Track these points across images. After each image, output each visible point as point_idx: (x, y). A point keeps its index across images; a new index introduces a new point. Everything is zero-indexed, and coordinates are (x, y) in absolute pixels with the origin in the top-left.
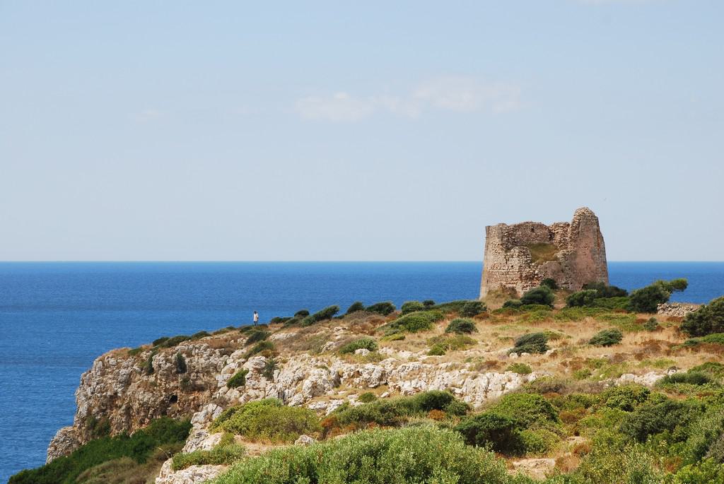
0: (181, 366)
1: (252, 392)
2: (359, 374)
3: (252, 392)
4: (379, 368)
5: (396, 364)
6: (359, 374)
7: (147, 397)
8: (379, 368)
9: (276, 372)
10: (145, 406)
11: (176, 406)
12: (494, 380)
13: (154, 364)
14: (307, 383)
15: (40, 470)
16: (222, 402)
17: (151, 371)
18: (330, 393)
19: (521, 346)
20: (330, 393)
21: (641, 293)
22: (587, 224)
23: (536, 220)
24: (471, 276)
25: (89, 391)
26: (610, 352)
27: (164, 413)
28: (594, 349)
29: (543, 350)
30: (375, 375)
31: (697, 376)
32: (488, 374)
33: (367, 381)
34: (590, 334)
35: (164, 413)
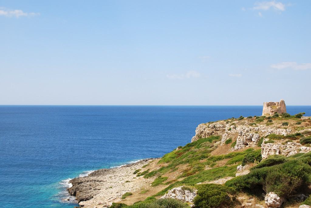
0: (214, 127)
1: (232, 131)
2: (254, 129)
3: (232, 131)
4: (258, 128)
5: (261, 127)
6: (254, 129)
7: (208, 132)
8: (258, 128)
9: (236, 128)
10: (208, 133)
11: (213, 133)
12: (280, 130)
13: (210, 126)
15: (274, 165)
16: (227, 133)
17: (209, 127)
18: (250, 132)
19: (283, 124)
20: (250, 132)
21: (298, 115)
22: (283, 102)
23: (273, 102)
24: (260, 109)
25: (198, 130)
27: (212, 135)
28: (297, 125)
29: (287, 125)
30: (257, 129)
31: (306, 131)
32: (279, 129)
33: (256, 130)
35: (212, 135)
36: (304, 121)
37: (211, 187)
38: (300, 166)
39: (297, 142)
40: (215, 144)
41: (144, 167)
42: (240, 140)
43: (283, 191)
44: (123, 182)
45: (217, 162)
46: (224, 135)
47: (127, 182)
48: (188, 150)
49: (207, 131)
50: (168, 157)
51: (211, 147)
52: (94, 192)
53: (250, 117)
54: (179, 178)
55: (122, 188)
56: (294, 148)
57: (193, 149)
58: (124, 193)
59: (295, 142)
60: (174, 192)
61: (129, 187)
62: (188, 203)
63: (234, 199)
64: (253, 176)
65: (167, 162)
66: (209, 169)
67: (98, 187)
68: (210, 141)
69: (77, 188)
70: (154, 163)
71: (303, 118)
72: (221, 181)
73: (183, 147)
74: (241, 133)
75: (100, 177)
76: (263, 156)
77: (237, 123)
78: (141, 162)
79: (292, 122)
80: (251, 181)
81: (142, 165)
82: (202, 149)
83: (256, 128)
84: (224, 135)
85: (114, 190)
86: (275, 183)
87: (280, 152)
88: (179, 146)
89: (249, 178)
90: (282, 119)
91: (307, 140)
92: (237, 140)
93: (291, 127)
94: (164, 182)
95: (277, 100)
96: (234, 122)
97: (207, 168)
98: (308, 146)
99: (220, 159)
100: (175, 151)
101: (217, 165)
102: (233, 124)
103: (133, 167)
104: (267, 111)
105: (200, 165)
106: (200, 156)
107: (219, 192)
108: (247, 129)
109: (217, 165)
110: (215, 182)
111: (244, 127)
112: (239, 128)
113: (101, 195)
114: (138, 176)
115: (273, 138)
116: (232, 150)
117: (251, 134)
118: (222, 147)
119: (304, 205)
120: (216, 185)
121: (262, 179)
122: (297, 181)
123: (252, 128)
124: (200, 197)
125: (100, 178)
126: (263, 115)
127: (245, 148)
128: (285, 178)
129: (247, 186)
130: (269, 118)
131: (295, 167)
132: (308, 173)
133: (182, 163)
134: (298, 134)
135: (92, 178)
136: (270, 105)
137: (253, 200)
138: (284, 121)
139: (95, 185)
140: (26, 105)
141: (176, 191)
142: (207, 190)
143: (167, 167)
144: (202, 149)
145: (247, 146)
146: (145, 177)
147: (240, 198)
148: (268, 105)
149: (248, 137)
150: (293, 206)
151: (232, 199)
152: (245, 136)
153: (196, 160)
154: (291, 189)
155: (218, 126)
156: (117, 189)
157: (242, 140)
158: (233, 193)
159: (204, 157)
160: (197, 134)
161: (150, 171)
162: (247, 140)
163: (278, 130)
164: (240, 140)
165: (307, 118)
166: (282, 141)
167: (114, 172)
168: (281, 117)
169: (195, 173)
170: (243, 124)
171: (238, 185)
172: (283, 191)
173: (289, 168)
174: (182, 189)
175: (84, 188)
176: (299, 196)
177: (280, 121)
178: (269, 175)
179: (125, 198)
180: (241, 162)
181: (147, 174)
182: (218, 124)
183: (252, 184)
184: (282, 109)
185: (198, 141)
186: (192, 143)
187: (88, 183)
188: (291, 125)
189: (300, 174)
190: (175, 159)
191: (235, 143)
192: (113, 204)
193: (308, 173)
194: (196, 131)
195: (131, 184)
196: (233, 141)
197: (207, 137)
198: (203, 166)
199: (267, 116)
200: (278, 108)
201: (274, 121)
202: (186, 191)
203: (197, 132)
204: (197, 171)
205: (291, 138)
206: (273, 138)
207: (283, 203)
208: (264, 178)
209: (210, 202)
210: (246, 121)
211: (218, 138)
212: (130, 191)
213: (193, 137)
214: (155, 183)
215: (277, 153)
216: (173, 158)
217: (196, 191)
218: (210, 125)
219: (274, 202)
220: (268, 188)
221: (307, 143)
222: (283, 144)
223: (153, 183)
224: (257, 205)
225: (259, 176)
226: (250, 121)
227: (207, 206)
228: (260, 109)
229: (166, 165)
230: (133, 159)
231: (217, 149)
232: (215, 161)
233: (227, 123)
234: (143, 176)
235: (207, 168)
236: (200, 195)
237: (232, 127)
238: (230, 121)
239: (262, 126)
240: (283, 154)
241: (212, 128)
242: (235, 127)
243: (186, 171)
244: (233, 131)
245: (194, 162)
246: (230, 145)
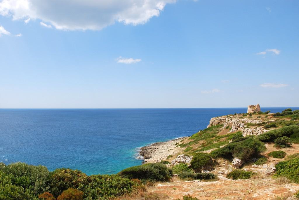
10: (217, 123)
14: (237, 121)
19: (258, 117)
22: (258, 105)
24: (246, 110)
26: (266, 118)
34: (264, 116)
36: (269, 115)
37: (201, 155)
38: (254, 142)
39: (263, 127)
40: (220, 129)
41: (181, 141)
42: (234, 127)
43: (243, 157)
44: (169, 149)
45: (220, 139)
46: (225, 124)
47: (171, 149)
48: (205, 132)
49: (216, 122)
50: (194, 136)
51: (218, 131)
52: (153, 154)
53: (240, 114)
54: (199, 148)
55: (168, 152)
56: (260, 131)
57: (208, 132)
58: (168, 155)
59: (261, 127)
60: (180, 157)
61: (172, 153)
62: (187, 164)
63: (215, 161)
64: (227, 148)
65: (193, 139)
66: (216, 143)
67: (155, 152)
68: (218, 127)
69: (145, 152)
70: (186, 139)
71: (269, 114)
72: (209, 152)
73: (203, 130)
74: (234, 123)
75: (157, 146)
76: (243, 135)
77: (233, 117)
78: (180, 139)
79: (262, 116)
80: (225, 151)
81: (180, 140)
82: (213, 132)
83: (243, 120)
84: (225, 124)
85: (164, 154)
86: (239, 152)
87: (252, 133)
88: (200, 130)
89: (224, 149)
90: (257, 115)
91: (268, 126)
92: (232, 126)
93: (262, 119)
94: (191, 150)
95: (255, 104)
96: (231, 117)
97: (215, 142)
98: (268, 130)
99: (222, 137)
100: (198, 133)
101: (221, 140)
102: (230, 118)
103: (175, 142)
104: (250, 110)
105: (211, 141)
106: (211, 136)
107: (205, 157)
108: (238, 120)
109: (221, 140)
110: (205, 152)
111: (236, 119)
112: (233, 120)
113: (156, 156)
114: (177, 146)
115: (250, 125)
116: (229, 132)
117: (240, 123)
118: (223, 131)
119: (255, 165)
120: (204, 153)
121: (231, 150)
122: (251, 151)
123: (240, 120)
124: (194, 160)
125: (157, 147)
126: (248, 112)
127: (236, 131)
128: (245, 149)
129: (223, 154)
130: (250, 114)
131: (251, 143)
132: (258, 146)
133: (201, 139)
134: (264, 123)
135: (153, 147)
136: (252, 107)
137: (226, 162)
138: (258, 116)
139: (154, 151)
140: (232, 108)
141: (181, 157)
142: (199, 156)
143: (193, 142)
144: (213, 132)
145: (238, 130)
146: (181, 147)
147: (219, 161)
148: (250, 107)
149: (238, 125)
150: (249, 166)
151: (214, 162)
152: (236, 125)
153: (209, 138)
154: (248, 155)
155: (222, 119)
156: (166, 153)
157: (235, 127)
158: (215, 158)
159: (213, 136)
160: (210, 123)
161: (184, 144)
162: (237, 126)
163: (255, 121)
164: (234, 127)
165: (271, 114)
166: (254, 127)
167: (165, 144)
168: (257, 113)
169: (208, 145)
170: (236, 118)
171: (218, 153)
172: (243, 157)
173: (247, 143)
174: (184, 155)
175: (148, 152)
176: (253, 159)
177: (256, 116)
178: (236, 148)
179: (168, 158)
180: (231, 139)
181: (182, 146)
182: (222, 118)
183: (226, 153)
184: (258, 109)
185: (211, 127)
186: (208, 128)
187: (151, 150)
188: (262, 118)
189: (253, 147)
190: (198, 137)
191: (231, 128)
192: (161, 161)
193: (258, 146)
194: (210, 122)
195: (173, 151)
196: (230, 127)
197: (216, 125)
198: (213, 141)
199: (249, 113)
200: (256, 108)
201: (253, 116)
202: (186, 157)
203: (210, 122)
204: (209, 144)
205: (260, 125)
206: (250, 125)
207: (243, 164)
208: (233, 149)
209: (200, 164)
210: (238, 116)
211: (222, 125)
212: (171, 154)
213: (208, 125)
214: (186, 151)
215: (251, 134)
216: (197, 137)
217: (192, 157)
218: (218, 119)
219: (237, 163)
220: (235, 155)
221: (268, 128)
222: (255, 128)
223: (185, 150)
224: (228, 165)
225: (230, 148)
226: (240, 116)
227: (198, 165)
228: (246, 110)
229: (193, 140)
230: (177, 137)
231: (221, 132)
232: (220, 138)
233: (227, 117)
234: (180, 146)
235: (215, 142)
236: (194, 159)
237: (229, 119)
238: (229, 116)
239: (246, 118)
240: (254, 134)
241: (219, 120)
242: (231, 119)
243: (203, 144)
244: (230, 122)
245: (208, 139)
246: (228, 129)
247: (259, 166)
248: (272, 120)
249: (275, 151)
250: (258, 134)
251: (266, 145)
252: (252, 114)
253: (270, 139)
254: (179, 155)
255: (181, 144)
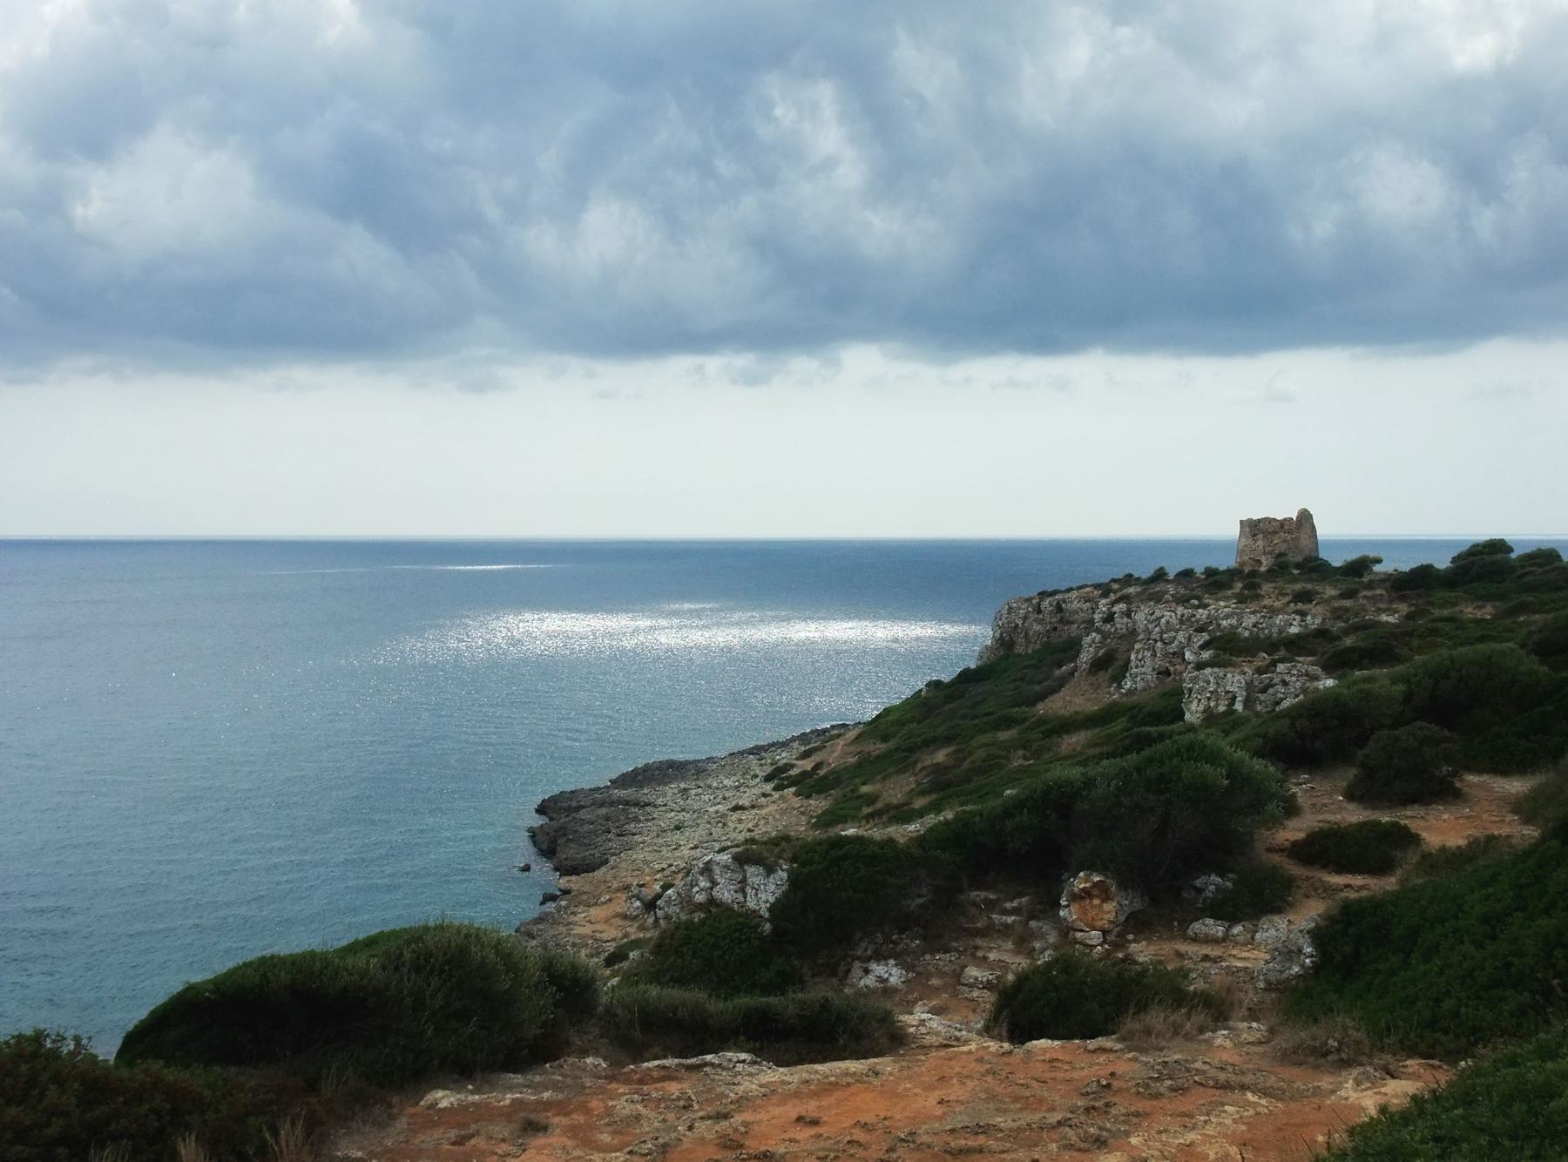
22: (1305, 517)
41: (805, 755)
47: (737, 808)
52: (615, 844)
69: (562, 831)
76: (1187, 716)
77: (1138, 595)
83: (1202, 614)
90: (1295, 580)
92: (1133, 657)
113: (639, 855)
125: (646, 793)
138: (1298, 587)
146: (796, 794)
149: (1173, 648)
152: (1159, 644)
159: (1007, 722)
161: (822, 773)
166: (1263, 658)
187: (604, 811)
202: (751, 870)
211: (1073, 647)
224: (1033, 924)
234: (793, 789)
244: (1121, 623)
247: (1237, 929)
248: (1384, 618)
249: (263, 958)
250: (1286, 704)
251: (1301, 787)
252: (1261, 575)
253: (1309, 741)
254: (707, 859)
255: (805, 774)
